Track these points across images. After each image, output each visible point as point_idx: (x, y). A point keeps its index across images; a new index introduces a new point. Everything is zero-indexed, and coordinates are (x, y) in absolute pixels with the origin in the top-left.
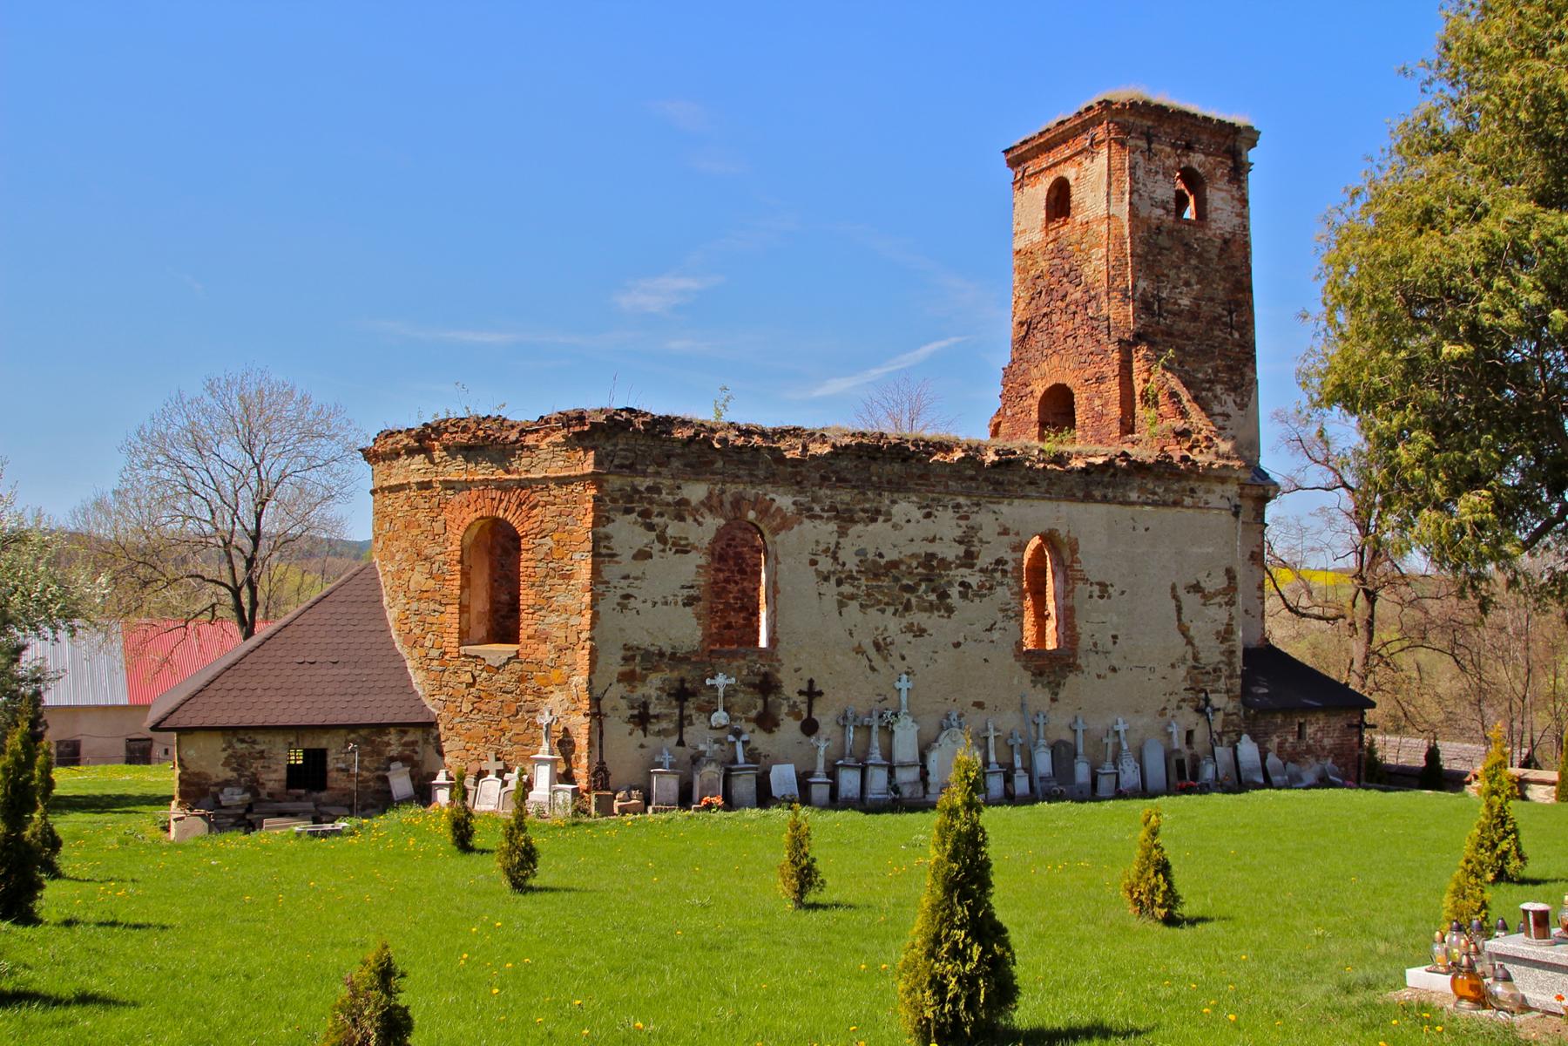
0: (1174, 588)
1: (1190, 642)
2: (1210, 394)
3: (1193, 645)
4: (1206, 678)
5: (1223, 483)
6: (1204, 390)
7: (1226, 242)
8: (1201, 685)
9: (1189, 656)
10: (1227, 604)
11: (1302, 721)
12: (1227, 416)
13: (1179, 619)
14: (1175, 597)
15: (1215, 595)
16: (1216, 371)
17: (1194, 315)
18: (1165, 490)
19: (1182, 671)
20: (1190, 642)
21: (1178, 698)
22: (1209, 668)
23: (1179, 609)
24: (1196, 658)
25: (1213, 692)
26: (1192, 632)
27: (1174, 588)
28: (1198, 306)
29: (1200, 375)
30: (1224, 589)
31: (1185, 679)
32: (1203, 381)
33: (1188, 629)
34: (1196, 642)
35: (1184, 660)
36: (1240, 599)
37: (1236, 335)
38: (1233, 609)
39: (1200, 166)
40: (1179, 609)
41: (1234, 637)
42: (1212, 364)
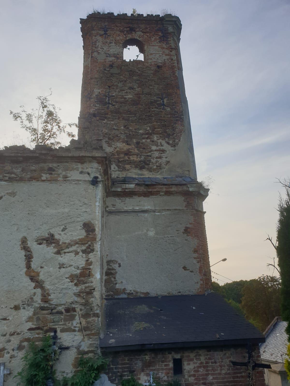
0: (24, 241)
1: (39, 284)
2: (149, 140)
3: (42, 288)
4: (56, 317)
5: (82, 163)
6: (144, 138)
7: (159, 67)
8: (51, 325)
9: (38, 298)
10: (84, 252)
11: (178, 356)
12: (163, 151)
13: (28, 266)
14: (26, 248)
15: (69, 245)
16: (153, 128)
17: (135, 102)
18: (23, 170)
19: (28, 313)
20: (39, 284)
21: (20, 337)
22: (61, 308)
23: (29, 258)
24: (45, 298)
25: (63, 331)
26: (42, 277)
27: (24, 241)
28: (139, 98)
29: (141, 131)
30: (81, 240)
31: (30, 319)
32: (143, 134)
33: (38, 274)
34: (47, 286)
35: (30, 302)
36: (97, 246)
37: (169, 109)
38: (91, 255)
39: (139, 37)
40: (29, 258)
41: (91, 279)
42: (150, 125)
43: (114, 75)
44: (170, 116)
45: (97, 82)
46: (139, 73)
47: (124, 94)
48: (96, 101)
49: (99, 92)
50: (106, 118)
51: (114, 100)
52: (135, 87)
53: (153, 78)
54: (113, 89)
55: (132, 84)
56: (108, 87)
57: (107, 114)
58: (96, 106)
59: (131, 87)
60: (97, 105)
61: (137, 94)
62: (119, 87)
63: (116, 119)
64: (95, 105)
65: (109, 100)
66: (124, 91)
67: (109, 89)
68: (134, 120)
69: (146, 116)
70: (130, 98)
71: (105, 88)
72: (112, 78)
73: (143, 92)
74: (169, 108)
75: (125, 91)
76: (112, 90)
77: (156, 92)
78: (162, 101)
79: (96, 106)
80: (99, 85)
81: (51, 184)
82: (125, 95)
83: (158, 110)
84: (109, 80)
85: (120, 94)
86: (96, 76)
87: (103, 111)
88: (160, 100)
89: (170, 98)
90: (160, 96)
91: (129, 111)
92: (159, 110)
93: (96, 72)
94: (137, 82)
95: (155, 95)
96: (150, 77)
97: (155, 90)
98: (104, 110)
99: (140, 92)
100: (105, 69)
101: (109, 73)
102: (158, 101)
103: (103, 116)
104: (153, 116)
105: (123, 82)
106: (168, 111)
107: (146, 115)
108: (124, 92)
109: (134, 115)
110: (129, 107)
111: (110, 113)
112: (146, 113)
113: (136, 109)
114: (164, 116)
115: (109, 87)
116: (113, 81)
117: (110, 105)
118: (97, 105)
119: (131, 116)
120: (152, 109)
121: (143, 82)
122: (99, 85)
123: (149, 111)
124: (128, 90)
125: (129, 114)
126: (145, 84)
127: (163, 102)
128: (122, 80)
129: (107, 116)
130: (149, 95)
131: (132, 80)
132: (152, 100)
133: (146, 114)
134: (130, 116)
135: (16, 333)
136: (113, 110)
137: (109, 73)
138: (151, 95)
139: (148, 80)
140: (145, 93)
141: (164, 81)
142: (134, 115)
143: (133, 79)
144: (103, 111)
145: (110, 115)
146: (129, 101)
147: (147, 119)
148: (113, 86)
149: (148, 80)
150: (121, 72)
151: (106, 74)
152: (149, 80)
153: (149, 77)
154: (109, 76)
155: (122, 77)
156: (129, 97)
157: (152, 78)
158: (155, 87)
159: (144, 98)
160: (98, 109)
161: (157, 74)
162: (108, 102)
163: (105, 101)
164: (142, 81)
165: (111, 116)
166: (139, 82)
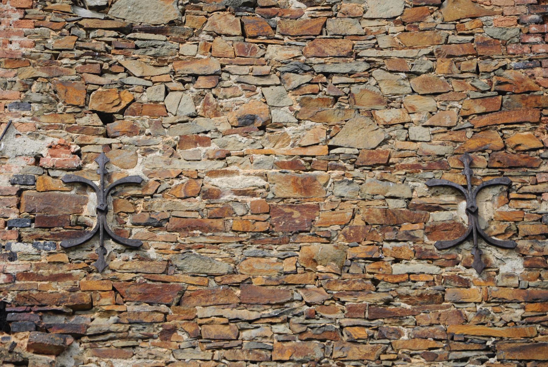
43: (138, 35)
44: (520, 312)
45: (26, 87)
46: (305, 17)
47: (202, 166)
48: (13, 216)
49: (38, 159)
50: (77, 337)
51: (140, 208)
52: (278, 116)
53: (403, 53)
54: (133, 131)
55: (258, 97)
56: (96, 120)
57: (89, 308)
58: (12, 257)
59: (253, 119)
60: (16, 247)
61: (294, 165)
62: (171, 118)
63: (146, 338)
64: (9, 246)
65: (102, 211)
66: (205, 142)
67: (106, 135)
68: (267, 343)
69: (352, 312)
70: (243, 193)
71: (83, 130)
72: (126, 56)
73: (331, 147)
74: (514, 255)
75: (214, 146)
76: (125, 139)
77: (427, 148)
78: (463, 205)
79: (12, 257)
80: (36, 107)
81: (19, 244)
82: (213, 173)
83: (434, 269)
84: (102, 73)
85: (178, 165)
86: (14, 47)
87: (61, 288)
88: (452, 198)
89: (524, 183)
90: (448, 177)
91: (237, 279)
92: (445, 272)
93: (18, 15)
94: (297, 80)
95: (416, 167)
96: (384, 41)
97: (416, 132)
98: (69, 283)
99: (310, 151)
100: (105, 122)
101: (109, 24)
102: (438, 208)
103: (61, 319)
104: (399, 317)
105: (202, 82)
106: (509, 276)
107: (351, 309)
108: (203, 150)
109: (271, 311)
110: (237, 257)
111: (106, 302)
112: (355, 292)
113: (288, 266)
114: (479, 314)
115: (107, 118)
116: (129, 75)
117: (111, 245)
118: (16, 247)
119: (254, 315)
120: (397, 261)
121: (336, 79)
122: (36, 107)
123: (375, 282)
124: (230, 139)
125: (239, 305)
126: (349, 94)
127: (472, 212)
128: (194, 68)
129: (84, 319)
130: (372, 168)
131: (259, 70)
132: (392, 204)
133: (350, 301)
134: (245, 314)
135: (117, 63)
136: (129, 277)
137: (109, 24)
138: (387, 165)
139: (365, 66)
140: (349, 158)
141: (477, 72)
142: (271, 311)
143: (268, 62)
144: (61, 288)
145: (108, 313)
146: (239, 210)
147: (362, 333)
148: (134, 113)
149: (365, 66)
150: (183, 13)
151: (89, 30)
152: (372, 64)
153: (376, 46)
154: (101, 47)
155: (188, 49)
156: (237, 187)
157: (395, 54)
158: (413, 111)
159: (340, 190)
160: (26, 275)
161: (430, 19)
162: (94, 223)
163: (73, 218)
164: (327, 75)
165: (113, 319)
166: (308, 77)
